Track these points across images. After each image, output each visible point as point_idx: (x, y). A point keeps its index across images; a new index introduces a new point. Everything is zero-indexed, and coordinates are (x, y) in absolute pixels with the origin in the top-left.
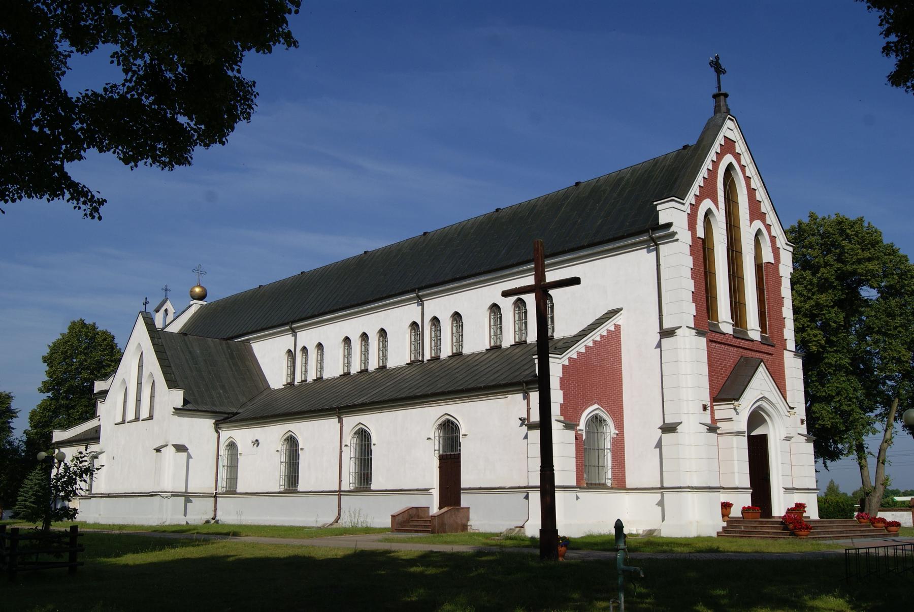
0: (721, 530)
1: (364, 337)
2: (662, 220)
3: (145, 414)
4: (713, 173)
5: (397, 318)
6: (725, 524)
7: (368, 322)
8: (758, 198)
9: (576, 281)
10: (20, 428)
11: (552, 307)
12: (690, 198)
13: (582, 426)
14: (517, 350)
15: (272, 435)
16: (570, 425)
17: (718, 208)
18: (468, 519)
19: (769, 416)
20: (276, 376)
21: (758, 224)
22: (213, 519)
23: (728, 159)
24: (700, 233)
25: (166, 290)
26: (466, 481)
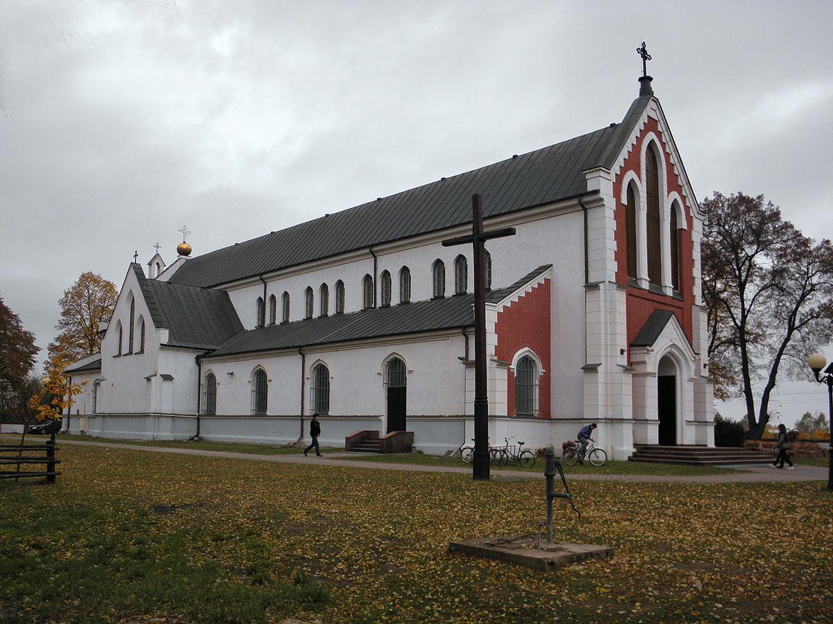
0: (631, 455)
1: (324, 287)
2: (590, 188)
3: (136, 348)
4: (637, 148)
5: (353, 274)
6: (635, 450)
7: (328, 276)
8: (676, 172)
9: (510, 232)
10: (39, 370)
11: (490, 275)
12: (616, 169)
13: (514, 366)
14: (458, 300)
15: (244, 370)
16: (503, 360)
17: (640, 179)
18: (412, 441)
19: (679, 364)
20: (249, 321)
21: (675, 195)
22: (196, 436)
23: (651, 136)
24: (624, 201)
25: (157, 247)
26: (412, 408)
